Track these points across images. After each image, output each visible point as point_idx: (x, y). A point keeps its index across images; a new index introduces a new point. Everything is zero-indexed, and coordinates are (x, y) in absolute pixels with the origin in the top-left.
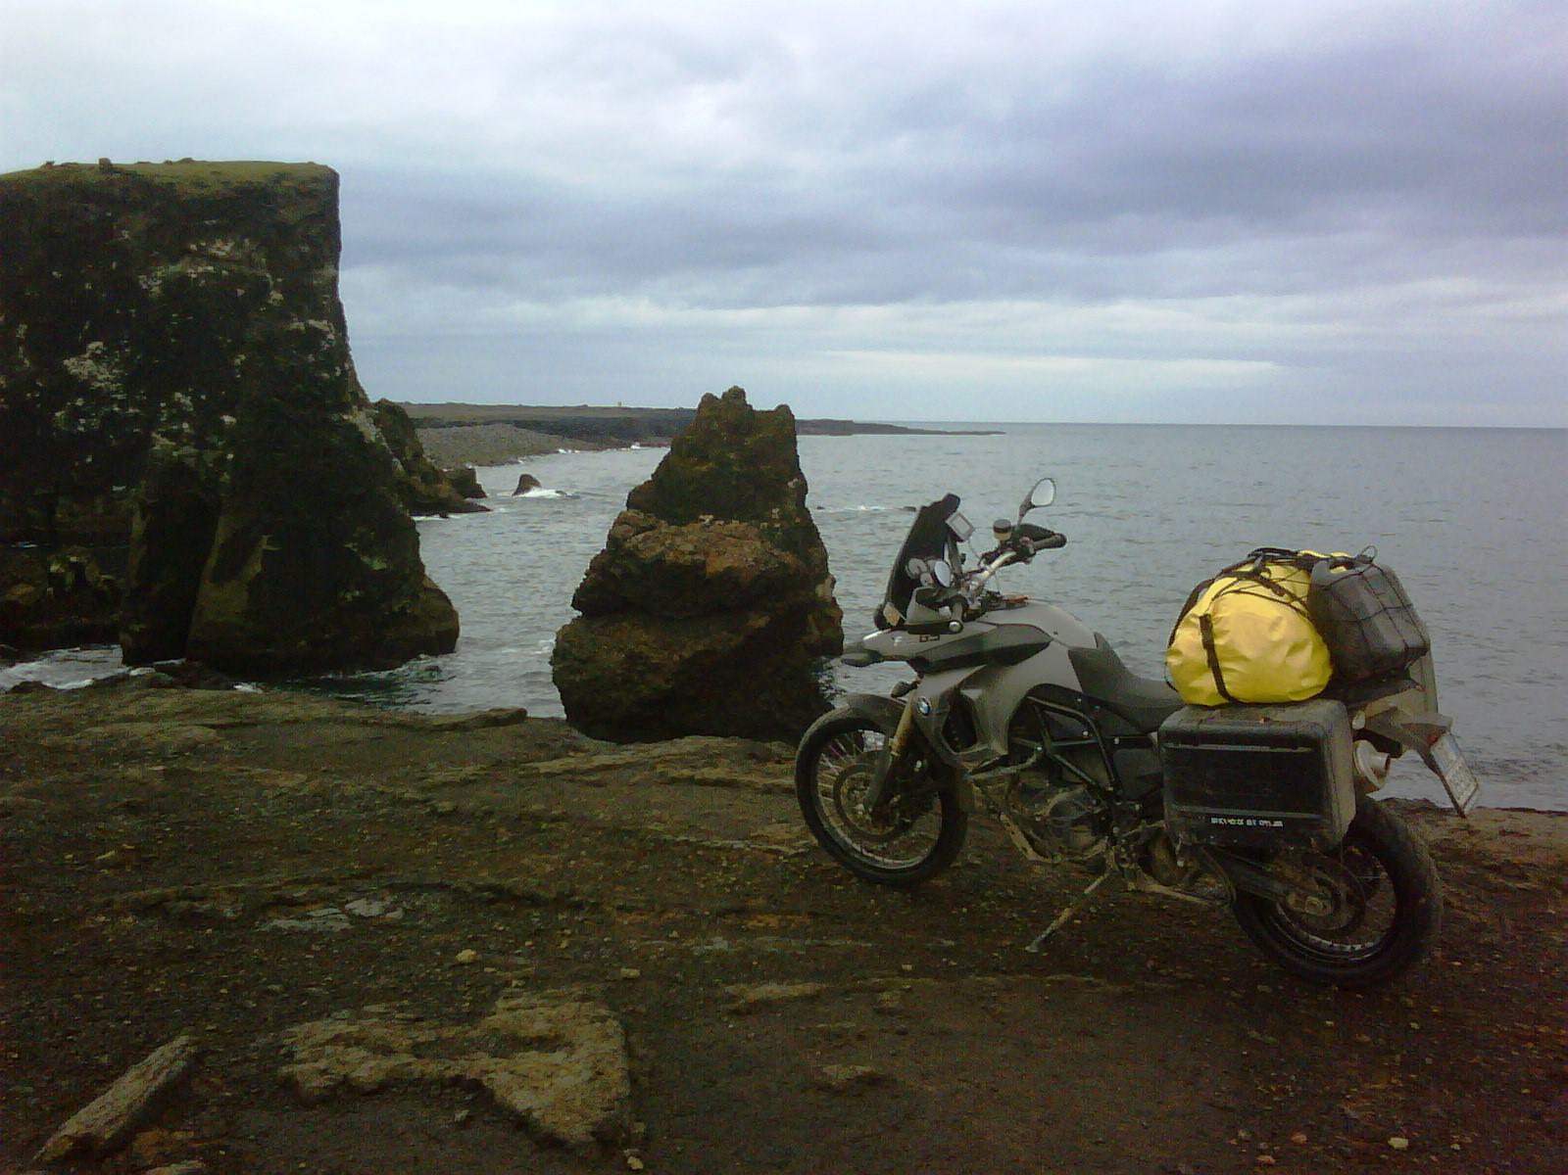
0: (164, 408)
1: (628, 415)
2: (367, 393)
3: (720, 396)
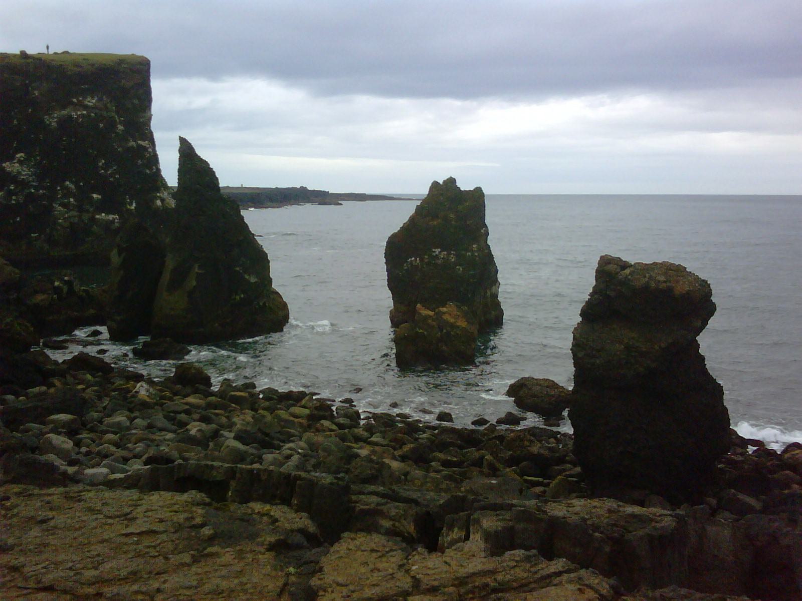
0: (59, 190)
1: (258, 191)
2: (166, 181)
3: (441, 183)
